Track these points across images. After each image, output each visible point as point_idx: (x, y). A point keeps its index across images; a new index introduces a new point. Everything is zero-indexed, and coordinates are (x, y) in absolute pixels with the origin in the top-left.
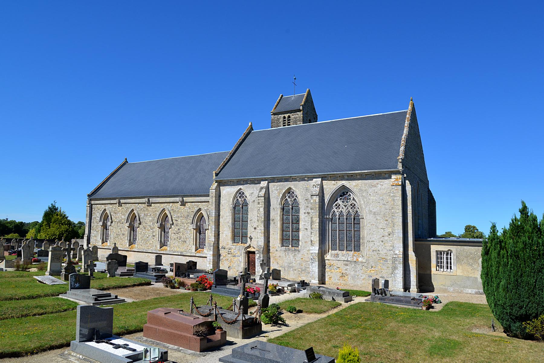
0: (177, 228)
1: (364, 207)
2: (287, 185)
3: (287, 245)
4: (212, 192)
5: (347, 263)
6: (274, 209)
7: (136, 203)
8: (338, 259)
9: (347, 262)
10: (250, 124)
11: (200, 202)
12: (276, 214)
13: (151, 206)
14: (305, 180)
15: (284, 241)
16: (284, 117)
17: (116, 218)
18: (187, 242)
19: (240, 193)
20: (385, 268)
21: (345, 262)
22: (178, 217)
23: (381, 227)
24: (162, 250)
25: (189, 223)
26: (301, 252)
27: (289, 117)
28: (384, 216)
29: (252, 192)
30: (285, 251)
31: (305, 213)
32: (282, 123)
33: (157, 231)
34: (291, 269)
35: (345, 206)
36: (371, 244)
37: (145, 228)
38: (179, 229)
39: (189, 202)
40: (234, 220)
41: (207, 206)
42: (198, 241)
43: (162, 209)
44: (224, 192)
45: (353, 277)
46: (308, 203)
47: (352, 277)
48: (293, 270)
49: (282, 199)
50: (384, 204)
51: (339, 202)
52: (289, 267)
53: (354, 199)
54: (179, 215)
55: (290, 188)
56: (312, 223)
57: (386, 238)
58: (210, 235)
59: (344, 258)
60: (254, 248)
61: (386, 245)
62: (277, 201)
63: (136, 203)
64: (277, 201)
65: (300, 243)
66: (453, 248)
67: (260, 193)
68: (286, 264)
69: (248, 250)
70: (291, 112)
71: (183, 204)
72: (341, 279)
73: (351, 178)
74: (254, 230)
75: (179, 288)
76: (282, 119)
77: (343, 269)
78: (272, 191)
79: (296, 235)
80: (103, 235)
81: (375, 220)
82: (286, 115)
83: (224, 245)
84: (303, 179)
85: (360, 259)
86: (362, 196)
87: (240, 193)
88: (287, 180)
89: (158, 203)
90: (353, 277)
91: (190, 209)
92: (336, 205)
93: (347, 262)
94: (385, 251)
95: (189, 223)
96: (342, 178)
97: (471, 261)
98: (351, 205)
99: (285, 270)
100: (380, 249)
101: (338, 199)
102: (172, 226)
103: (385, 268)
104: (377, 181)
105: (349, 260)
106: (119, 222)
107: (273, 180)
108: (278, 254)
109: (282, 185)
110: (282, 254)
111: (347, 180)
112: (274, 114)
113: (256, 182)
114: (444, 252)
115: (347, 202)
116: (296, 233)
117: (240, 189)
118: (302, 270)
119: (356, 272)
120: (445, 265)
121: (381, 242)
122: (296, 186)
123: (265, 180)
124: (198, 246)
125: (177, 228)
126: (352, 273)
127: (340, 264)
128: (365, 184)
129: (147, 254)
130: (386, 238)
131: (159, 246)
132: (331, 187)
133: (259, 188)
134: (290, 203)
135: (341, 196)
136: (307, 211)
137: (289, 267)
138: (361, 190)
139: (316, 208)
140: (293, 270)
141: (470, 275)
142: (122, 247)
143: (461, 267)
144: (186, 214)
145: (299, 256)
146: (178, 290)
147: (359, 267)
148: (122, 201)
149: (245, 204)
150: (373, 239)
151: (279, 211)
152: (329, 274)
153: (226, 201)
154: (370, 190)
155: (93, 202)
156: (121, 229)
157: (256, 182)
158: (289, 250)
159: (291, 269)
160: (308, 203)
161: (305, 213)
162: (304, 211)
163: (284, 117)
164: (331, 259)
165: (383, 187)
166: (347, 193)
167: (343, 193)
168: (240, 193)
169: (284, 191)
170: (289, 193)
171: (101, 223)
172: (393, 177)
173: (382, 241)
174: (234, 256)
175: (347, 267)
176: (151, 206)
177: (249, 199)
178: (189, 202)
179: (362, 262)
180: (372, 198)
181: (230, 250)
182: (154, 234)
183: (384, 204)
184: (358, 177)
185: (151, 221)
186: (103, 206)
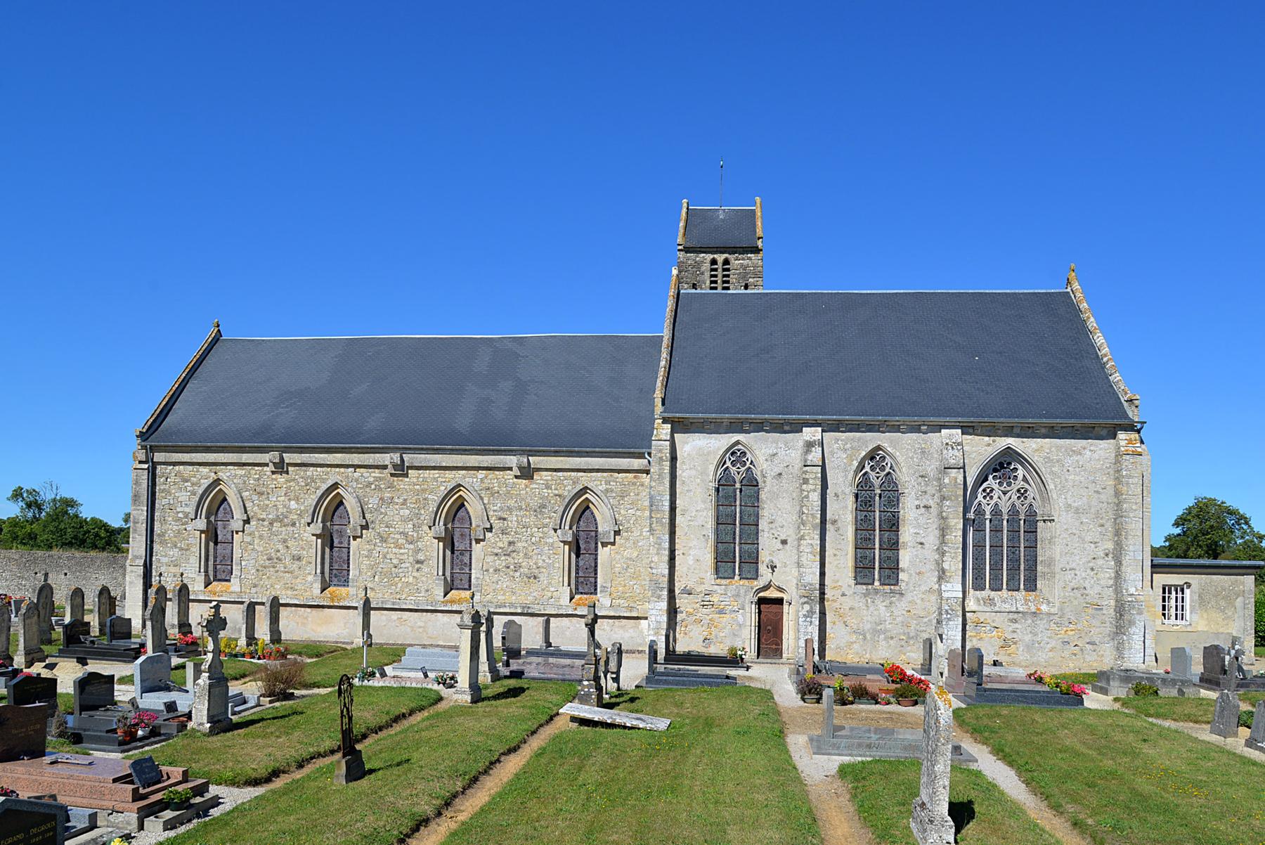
0: (506, 539)
1: (1055, 496)
2: (872, 440)
3: (866, 580)
4: (660, 446)
5: (1016, 616)
6: (836, 495)
7: (348, 466)
8: (997, 609)
9: (1016, 616)
10: (675, 272)
11: (584, 471)
12: (843, 510)
13: (406, 475)
14: (919, 431)
15: (863, 570)
16: (714, 262)
17: (264, 508)
18: (542, 577)
19: (737, 454)
20: (1098, 624)
21: (1011, 616)
22: (510, 509)
23: (1088, 539)
24: (452, 602)
25: (545, 526)
26: (909, 597)
27: (726, 262)
28: (1098, 515)
29: (773, 454)
30: (865, 595)
31: (918, 507)
32: (707, 274)
33: (433, 549)
34: (882, 636)
35: (1005, 493)
36: (1069, 576)
37: (384, 540)
38: (510, 543)
39: (547, 470)
40: (723, 521)
41: (608, 483)
42: (211, 563)
43: (330, 483)
44: (687, 448)
45: (1029, 648)
46: (927, 485)
47: (1028, 646)
48: (885, 639)
49: (856, 473)
50: (1098, 492)
51: (991, 482)
52: (876, 632)
53: (1025, 479)
54: (511, 503)
55: (879, 448)
56: (943, 531)
57: (1100, 562)
58: (656, 559)
59: (1007, 607)
60: (780, 589)
61: (1101, 575)
62: (846, 476)
63: (348, 466)
64: (846, 476)
65: (901, 576)
66: (1194, 579)
67: (810, 457)
68: (869, 626)
69: (762, 594)
70: (733, 250)
71: (527, 473)
72: (1002, 652)
73: (1028, 432)
74: (781, 546)
75: (852, 703)
76: (707, 266)
77: (1008, 630)
78: (832, 453)
79: (889, 558)
80: (207, 560)
81: (1077, 524)
82: (720, 258)
83: (690, 585)
84: (916, 429)
85: (1044, 608)
86: (1052, 473)
87: (733, 454)
88: (871, 428)
89: (434, 468)
90: (1029, 648)
91: (548, 487)
92: (984, 490)
93: (1016, 616)
94: (1097, 589)
95: (545, 526)
96: (1009, 432)
97: (1223, 603)
98: (1018, 491)
99: (865, 638)
100: (1087, 585)
101: (991, 477)
102: (488, 535)
103: (1096, 623)
104: (1084, 442)
105: (1021, 609)
106: (278, 519)
107: (835, 427)
108: (847, 603)
109: (859, 439)
110: (859, 603)
111: (1018, 436)
112: (687, 250)
113: (786, 428)
114: (1176, 587)
115: (1009, 484)
116: (888, 553)
117: (738, 443)
118: (909, 638)
119: (1036, 635)
120: (1173, 611)
121: (1089, 571)
122: (893, 443)
123: (815, 424)
124: (573, 586)
125: (506, 539)
126: (1028, 638)
127: (1000, 620)
128: (1059, 448)
129: (395, 615)
130: (1100, 562)
131: (440, 591)
132: (982, 449)
133: (801, 443)
134: (877, 483)
135: (995, 470)
136: (925, 502)
137: (876, 632)
138: (1048, 460)
139: (957, 497)
140: (885, 639)
141: (1221, 630)
142: (295, 597)
143: (1205, 616)
144: (534, 503)
145: (901, 605)
146: (854, 706)
147: (1042, 624)
148: (288, 458)
149: (751, 483)
150: (1074, 565)
151: (850, 503)
152: (975, 640)
153: (693, 472)
154: (1069, 461)
155: (158, 457)
156: (285, 541)
157: (786, 428)
158: (876, 591)
159: (882, 636)
160: (927, 485)
161: (918, 507)
162: (917, 503)
163: (714, 262)
164: (981, 608)
165: (1096, 456)
166: (1009, 464)
167: (1001, 465)
168: (737, 454)
169: (864, 453)
170: (872, 459)
171: (201, 524)
172: (1122, 435)
173: (1092, 569)
174: (721, 612)
175: (1017, 625)
176: (406, 475)
177: (906, 478)
178: (547, 470)
179: (1049, 614)
180: (1072, 477)
181: (708, 598)
182: (421, 557)
183: (1098, 492)
184: (1043, 431)
185: (405, 520)
186: (205, 470)
